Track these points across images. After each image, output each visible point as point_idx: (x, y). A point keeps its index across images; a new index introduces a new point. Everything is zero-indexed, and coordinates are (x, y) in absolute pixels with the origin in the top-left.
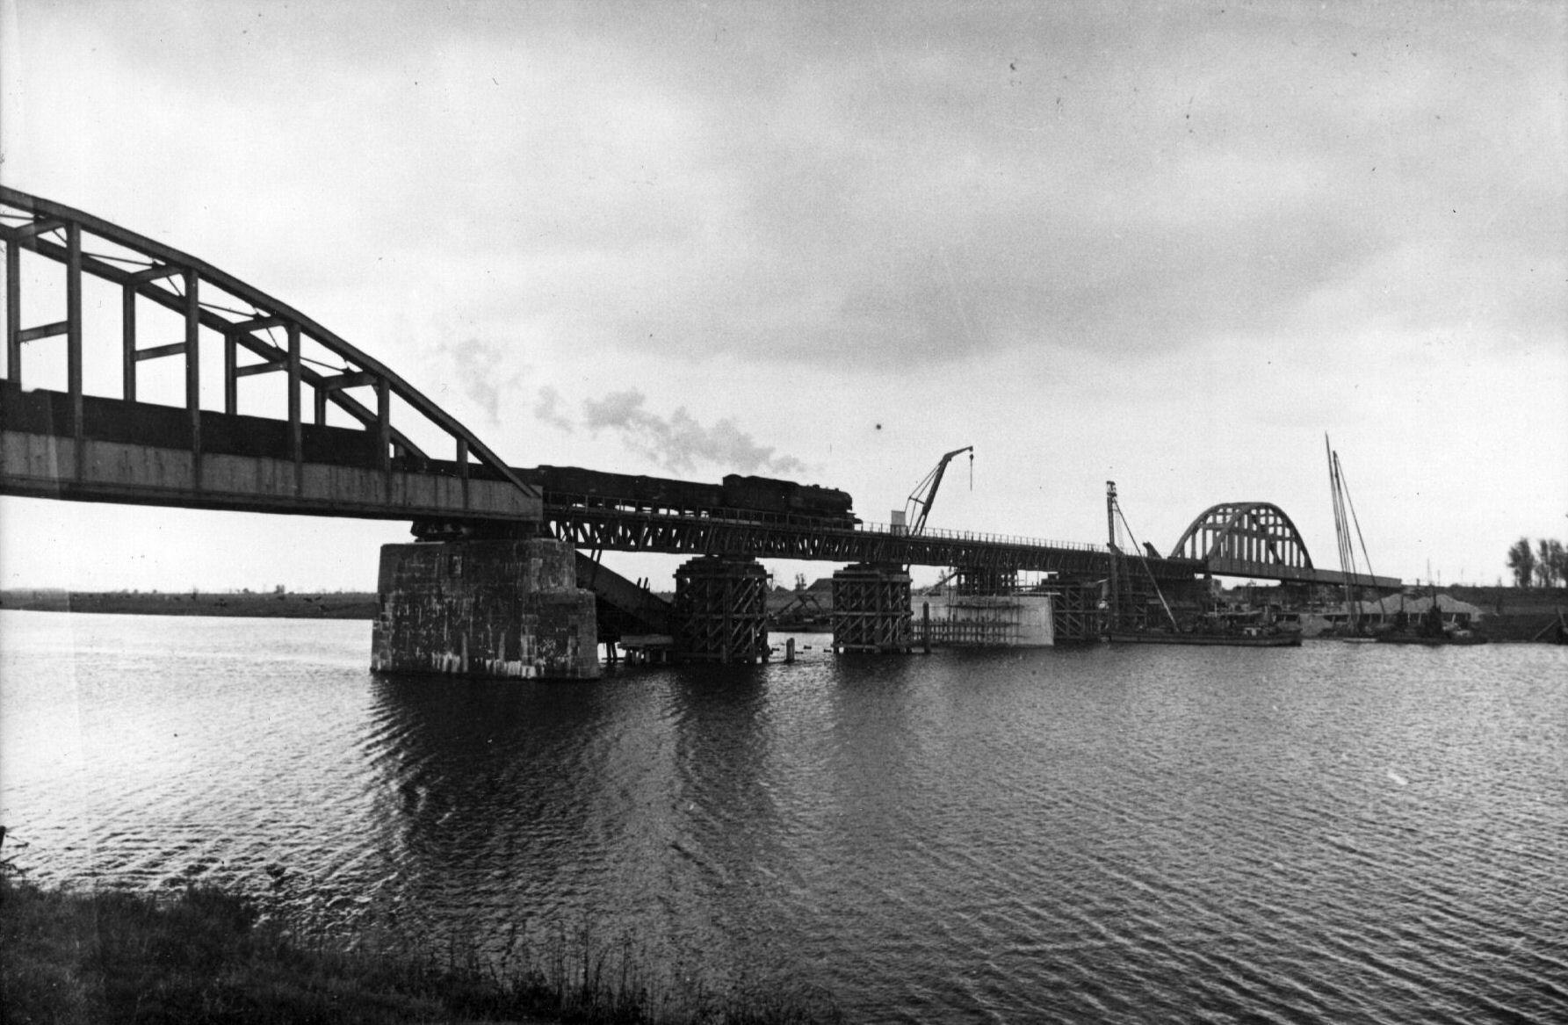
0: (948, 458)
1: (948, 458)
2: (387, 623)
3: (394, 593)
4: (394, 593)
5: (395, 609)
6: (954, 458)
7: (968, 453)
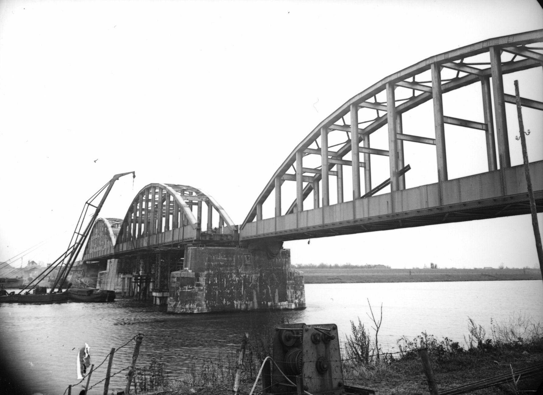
2: (202, 288)
3: (206, 273)
4: (206, 273)
5: (207, 280)
6: (120, 178)
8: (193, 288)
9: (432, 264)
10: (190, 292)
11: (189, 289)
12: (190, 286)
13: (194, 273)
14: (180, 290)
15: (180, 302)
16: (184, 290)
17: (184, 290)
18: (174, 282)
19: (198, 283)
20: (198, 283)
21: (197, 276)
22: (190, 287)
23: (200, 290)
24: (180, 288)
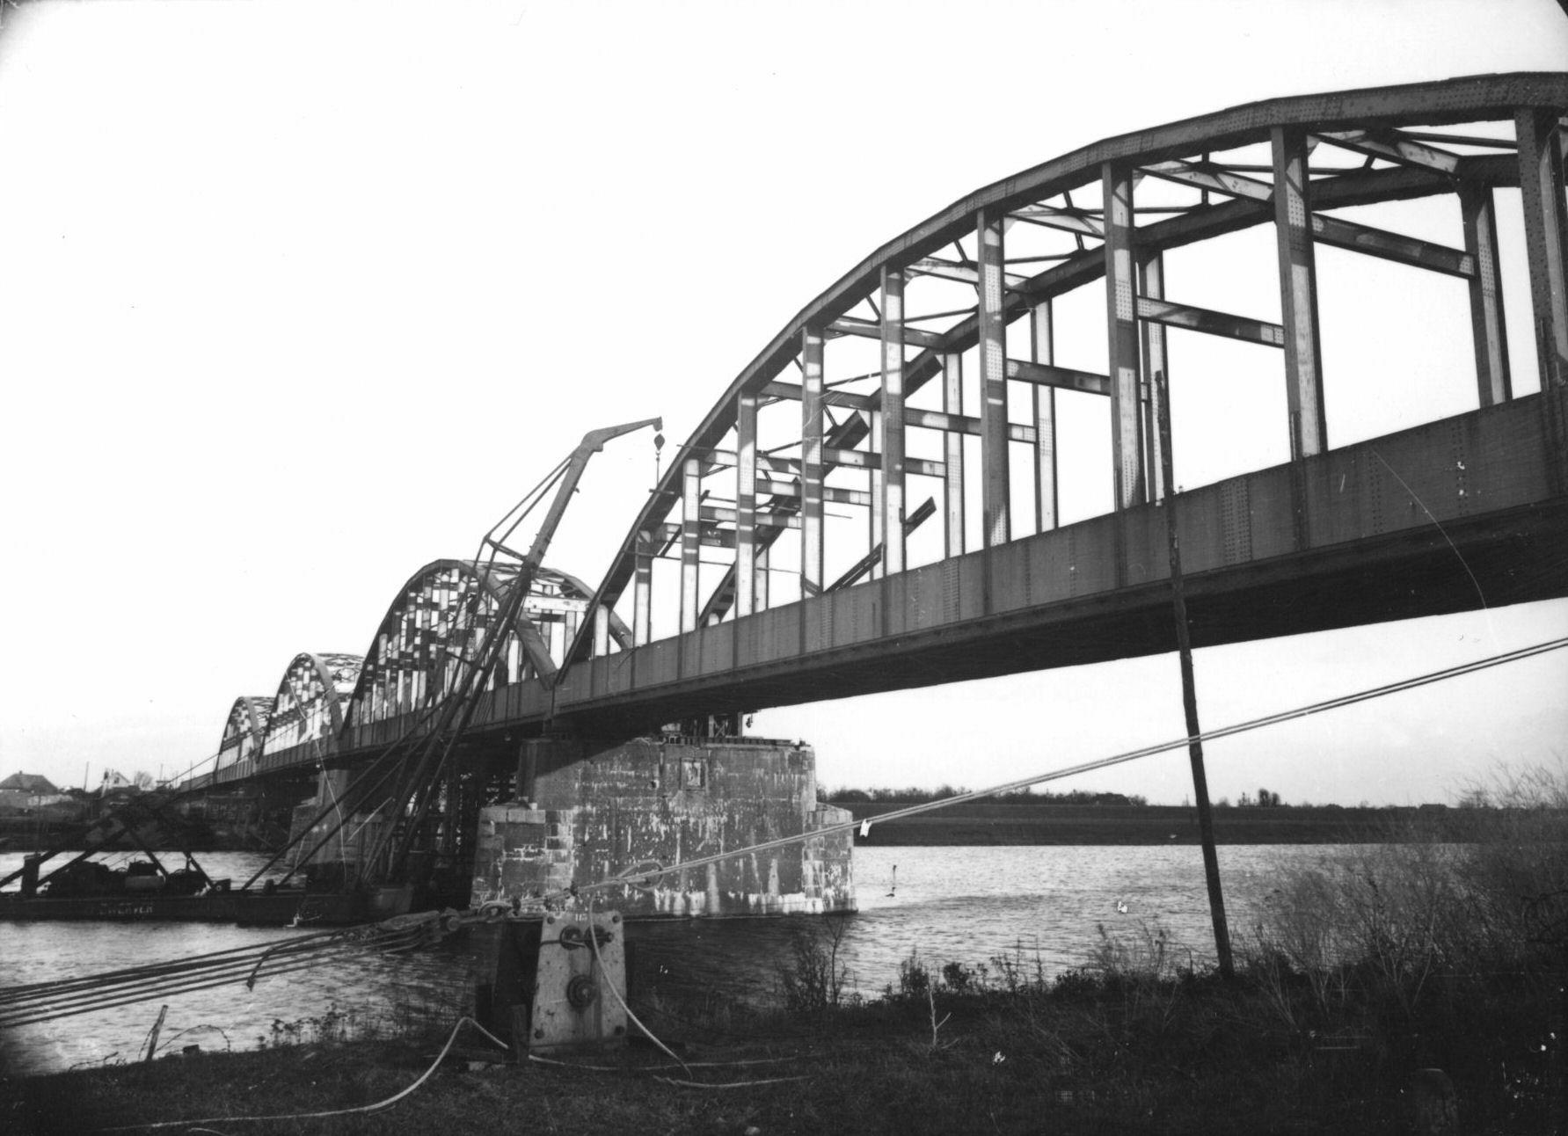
0: (594, 443)
1: (594, 443)
2: (564, 853)
7: (649, 433)
8: (540, 853)
9: (1263, 794)
10: (532, 863)
11: (528, 854)
12: (533, 848)
13: (544, 811)
14: (504, 859)
15: (503, 892)
16: (515, 859)
17: (515, 859)
18: (490, 836)
19: (554, 838)
20: (554, 838)
21: (552, 819)
22: (532, 851)
23: (558, 859)
24: (505, 853)
